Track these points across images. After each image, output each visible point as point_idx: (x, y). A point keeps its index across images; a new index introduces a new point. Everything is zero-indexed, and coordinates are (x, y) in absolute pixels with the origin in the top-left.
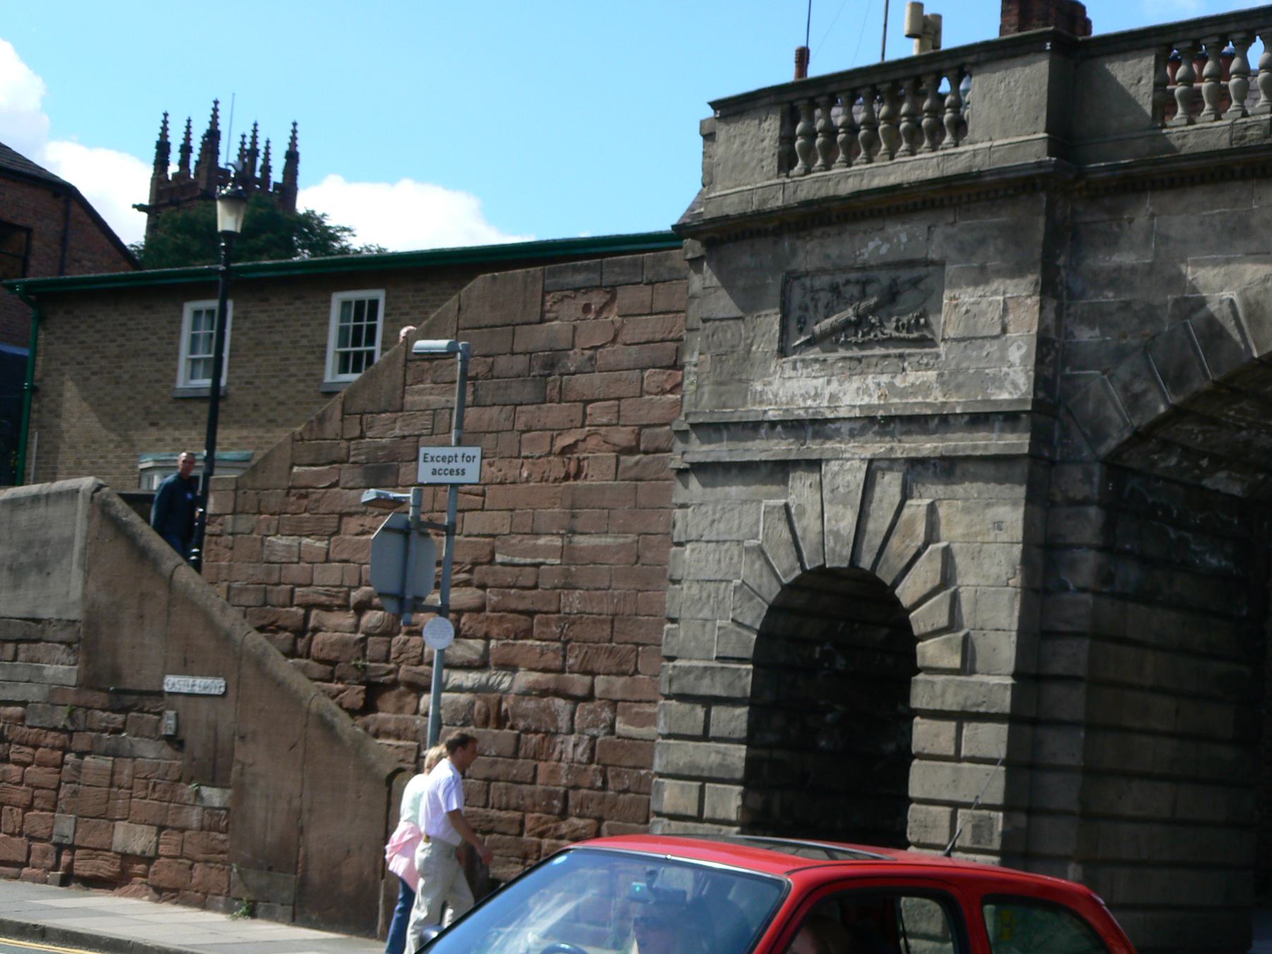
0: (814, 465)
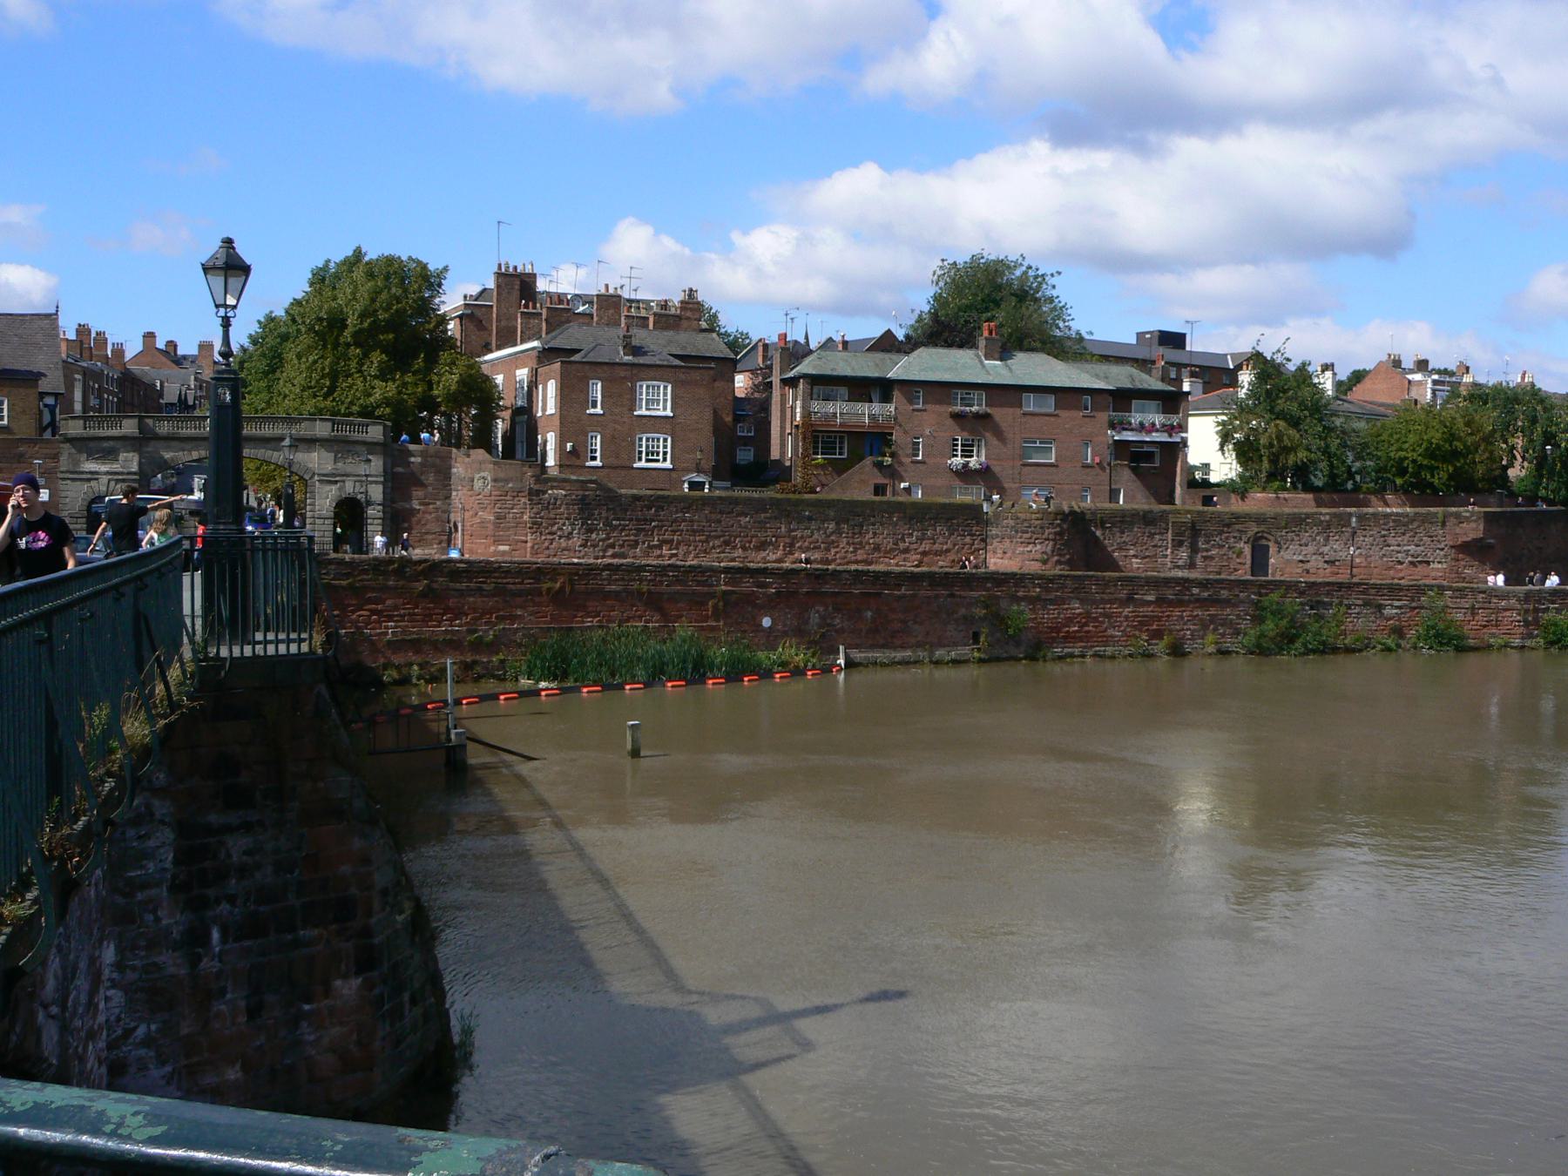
0: (97, 479)
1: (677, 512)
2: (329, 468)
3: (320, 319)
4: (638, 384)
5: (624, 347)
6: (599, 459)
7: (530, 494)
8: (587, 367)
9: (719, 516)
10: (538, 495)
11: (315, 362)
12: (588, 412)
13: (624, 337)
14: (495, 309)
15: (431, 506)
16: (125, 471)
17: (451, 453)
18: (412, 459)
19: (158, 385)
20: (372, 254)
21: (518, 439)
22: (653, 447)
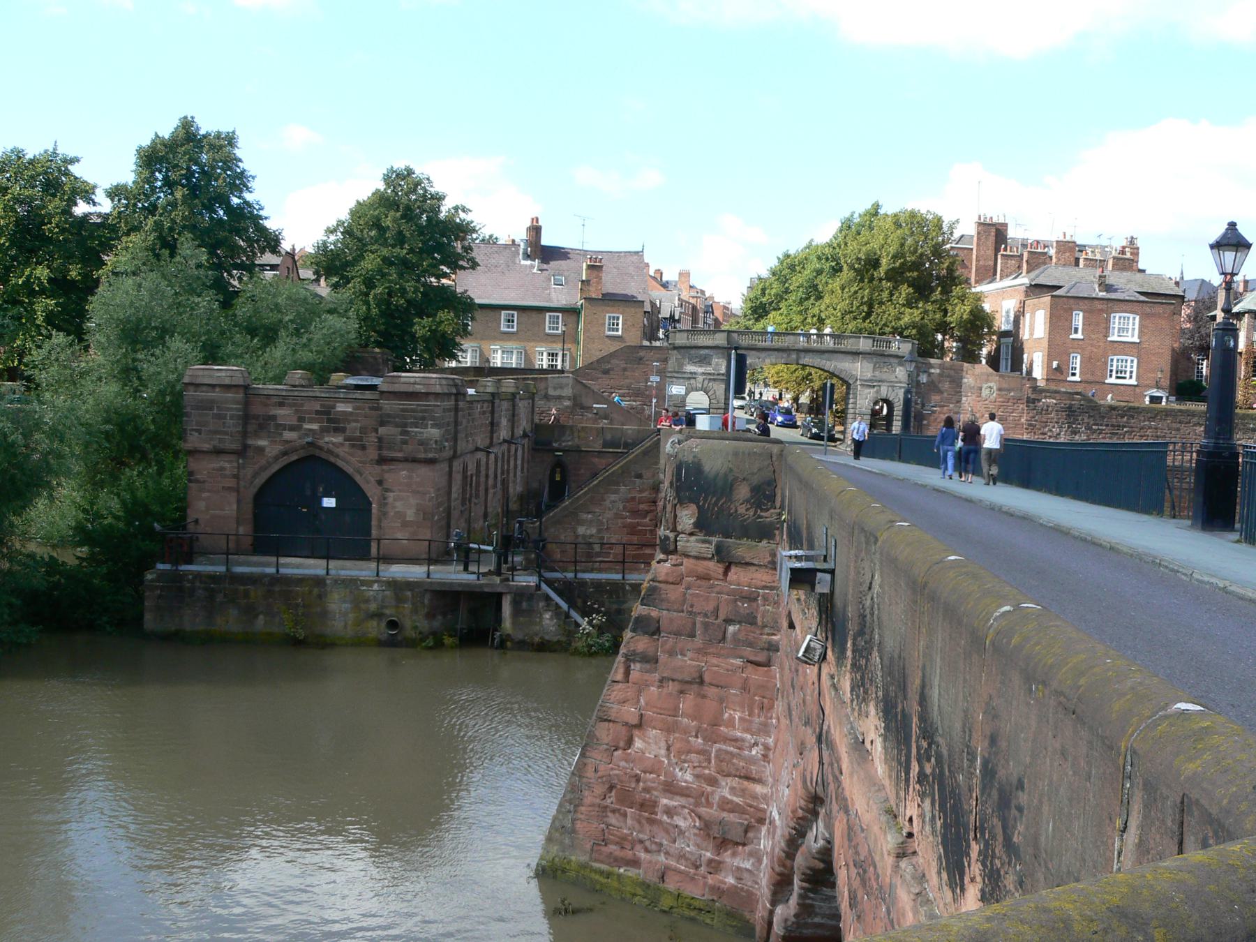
0: (695, 378)
1: (1144, 421)
2: (869, 375)
3: (858, 259)
4: (1112, 315)
5: (1100, 285)
6: (1078, 375)
7: (1028, 402)
8: (1072, 301)
9: (1179, 425)
10: (1034, 403)
11: (856, 292)
12: (1071, 337)
13: (1100, 277)
14: (974, 251)
15: (945, 408)
16: (716, 372)
17: (962, 366)
18: (932, 371)
19: (658, 304)
20: (889, 208)
21: (1003, 356)
22: (1122, 367)
